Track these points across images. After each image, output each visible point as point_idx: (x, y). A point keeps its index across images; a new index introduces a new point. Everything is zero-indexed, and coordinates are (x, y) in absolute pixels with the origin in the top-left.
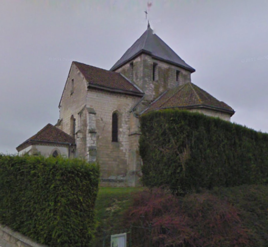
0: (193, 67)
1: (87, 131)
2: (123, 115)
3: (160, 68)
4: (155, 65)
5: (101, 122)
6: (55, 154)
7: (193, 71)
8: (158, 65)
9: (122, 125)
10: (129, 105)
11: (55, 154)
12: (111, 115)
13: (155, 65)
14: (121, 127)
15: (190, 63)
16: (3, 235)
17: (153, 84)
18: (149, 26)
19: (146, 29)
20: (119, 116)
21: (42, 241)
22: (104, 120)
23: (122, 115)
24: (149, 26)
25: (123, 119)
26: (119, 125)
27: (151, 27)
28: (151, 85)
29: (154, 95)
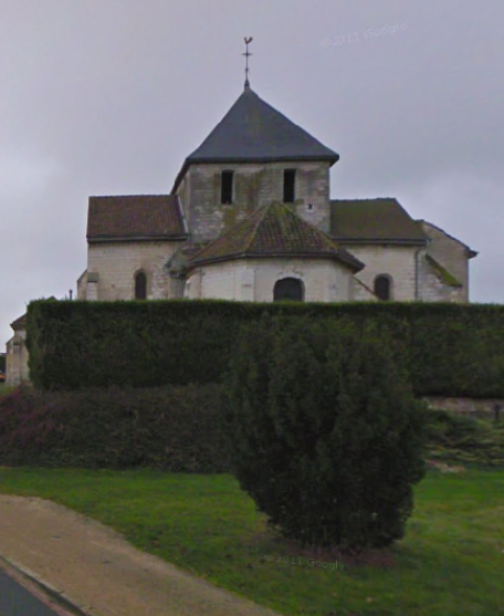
0: (336, 150)
1: (288, 271)
2: (154, 274)
3: (241, 176)
4: (227, 178)
5: (112, 290)
6: (288, 288)
7: (332, 159)
8: (235, 174)
9: (153, 289)
10: (162, 258)
11: (288, 288)
12: (132, 276)
13: (227, 178)
14: (151, 293)
15: (329, 142)
16: (416, 293)
17: (221, 210)
18: (247, 84)
19: (241, 90)
20: (148, 277)
21: (463, 292)
22: (117, 286)
23: (151, 274)
24: (247, 84)
25: (155, 282)
26: (148, 291)
27: (253, 87)
28: (217, 212)
29: (222, 230)
